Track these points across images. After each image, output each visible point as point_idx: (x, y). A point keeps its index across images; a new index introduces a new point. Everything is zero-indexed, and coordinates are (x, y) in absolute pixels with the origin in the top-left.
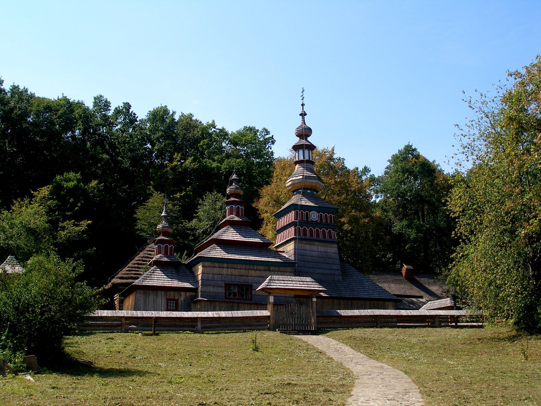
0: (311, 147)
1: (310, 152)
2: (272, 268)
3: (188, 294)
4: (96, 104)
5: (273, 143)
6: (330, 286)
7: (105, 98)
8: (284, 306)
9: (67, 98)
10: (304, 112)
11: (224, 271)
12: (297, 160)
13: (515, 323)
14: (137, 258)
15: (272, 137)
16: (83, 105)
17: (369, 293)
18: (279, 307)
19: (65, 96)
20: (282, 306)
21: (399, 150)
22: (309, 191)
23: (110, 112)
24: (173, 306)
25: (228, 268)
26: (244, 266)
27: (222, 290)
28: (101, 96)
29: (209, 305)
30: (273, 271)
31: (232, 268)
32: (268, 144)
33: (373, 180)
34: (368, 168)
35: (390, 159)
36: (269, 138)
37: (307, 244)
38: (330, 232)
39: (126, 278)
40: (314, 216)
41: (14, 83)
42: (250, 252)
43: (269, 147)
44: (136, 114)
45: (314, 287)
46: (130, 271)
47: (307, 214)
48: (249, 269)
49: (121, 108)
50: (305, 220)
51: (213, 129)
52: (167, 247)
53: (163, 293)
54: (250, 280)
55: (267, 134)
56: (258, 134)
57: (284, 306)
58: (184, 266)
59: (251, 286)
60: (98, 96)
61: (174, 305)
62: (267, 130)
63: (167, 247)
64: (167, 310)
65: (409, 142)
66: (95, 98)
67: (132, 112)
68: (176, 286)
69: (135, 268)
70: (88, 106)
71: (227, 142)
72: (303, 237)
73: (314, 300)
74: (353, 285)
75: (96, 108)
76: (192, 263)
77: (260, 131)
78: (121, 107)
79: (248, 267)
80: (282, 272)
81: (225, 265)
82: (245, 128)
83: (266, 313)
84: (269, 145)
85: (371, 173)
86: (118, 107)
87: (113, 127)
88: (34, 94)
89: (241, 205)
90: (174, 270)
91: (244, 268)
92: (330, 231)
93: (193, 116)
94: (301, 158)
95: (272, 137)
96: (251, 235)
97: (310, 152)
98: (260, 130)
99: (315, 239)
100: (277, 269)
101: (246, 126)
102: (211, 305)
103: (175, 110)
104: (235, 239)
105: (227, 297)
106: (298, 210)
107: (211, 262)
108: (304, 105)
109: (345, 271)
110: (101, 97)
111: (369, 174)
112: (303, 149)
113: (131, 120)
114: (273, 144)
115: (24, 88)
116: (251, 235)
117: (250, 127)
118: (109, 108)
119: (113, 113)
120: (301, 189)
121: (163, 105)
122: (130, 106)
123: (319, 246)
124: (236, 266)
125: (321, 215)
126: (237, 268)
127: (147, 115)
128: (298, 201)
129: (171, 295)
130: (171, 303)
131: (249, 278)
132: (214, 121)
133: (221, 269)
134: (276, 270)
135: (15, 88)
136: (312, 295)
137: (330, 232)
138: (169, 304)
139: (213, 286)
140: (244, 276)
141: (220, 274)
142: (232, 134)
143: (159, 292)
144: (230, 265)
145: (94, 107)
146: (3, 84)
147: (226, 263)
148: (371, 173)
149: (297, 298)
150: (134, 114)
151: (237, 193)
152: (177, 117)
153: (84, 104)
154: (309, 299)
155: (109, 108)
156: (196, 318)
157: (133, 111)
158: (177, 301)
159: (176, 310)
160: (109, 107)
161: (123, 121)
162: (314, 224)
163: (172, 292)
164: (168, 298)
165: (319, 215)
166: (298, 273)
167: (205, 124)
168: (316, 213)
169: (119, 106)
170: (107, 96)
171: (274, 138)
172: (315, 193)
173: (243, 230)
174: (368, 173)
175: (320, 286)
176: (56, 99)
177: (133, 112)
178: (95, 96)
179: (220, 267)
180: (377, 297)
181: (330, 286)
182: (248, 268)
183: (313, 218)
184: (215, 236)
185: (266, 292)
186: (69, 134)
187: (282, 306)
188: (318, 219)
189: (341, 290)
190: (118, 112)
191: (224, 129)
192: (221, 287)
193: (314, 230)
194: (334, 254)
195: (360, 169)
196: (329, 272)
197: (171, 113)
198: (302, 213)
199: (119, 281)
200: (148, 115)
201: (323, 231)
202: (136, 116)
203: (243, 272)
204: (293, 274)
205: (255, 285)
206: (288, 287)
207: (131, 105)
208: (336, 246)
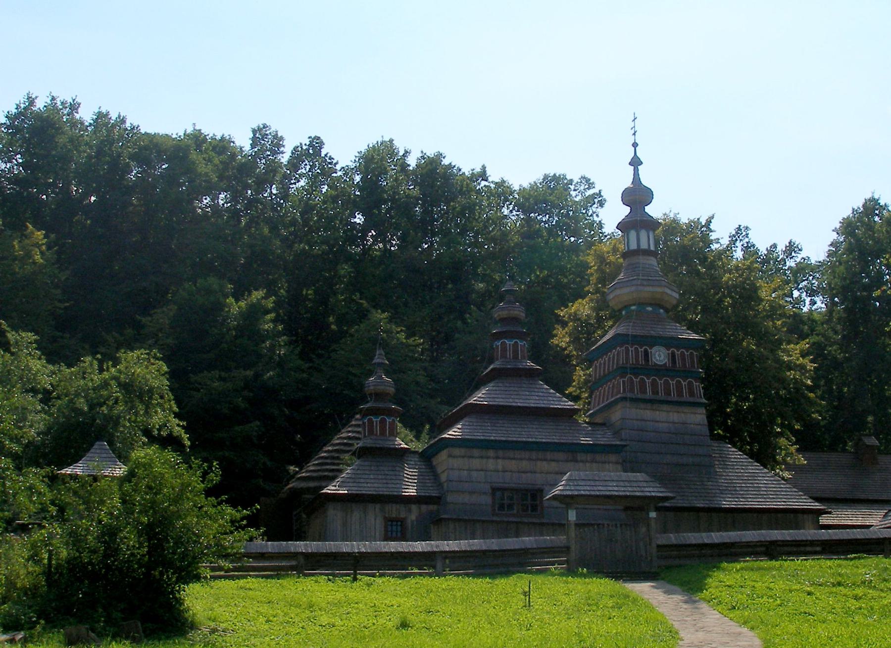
2: (580, 456)
3: (424, 508)
4: (255, 142)
5: (601, 204)
6: (693, 487)
9: (202, 132)
11: (491, 464)
15: (599, 194)
16: (232, 144)
19: (197, 128)
21: (853, 209)
22: (650, 309)
23: (283, 157)
25: (497, 458)
26: (527, 454)
27: (487, 500)
28: (265, 126)
30: (582, 461)
31: (504, 458)
32: (591, 206)
33: (804, 269)
34: (797, 243)
35: (838, 227)
36: (593, 196)
37: (647, 409)
38: (690, 383)
41: (100, 108)
43: (594, 213)
44: (333, 159)
48: (538, 459)
49: (304, 147)
51: (483, 183)
53: (378, 506)
54: (539, 480)
55: (589, 188)
56: (572, 187)
58: (417, 456)
60: (259, 127)
61: (399, 528)
62: (590, 180)
64: (387, 538)
65: (873, 193)
66: (254, 132)
67: (326, 155)
70: (242, 146)
71: (511, 207)
72: (639, 396)
73: (653, 515)
75: (256, 150)
77: (575, 182)
78: (305, 145)
79: (534, 455)
80: (599, 462)
81: (491, 453)
82: (546, 177)
84: (594, 210)
85: (803, 254)
86: (299, 145)
87: (292, 184)
88: (138, 126)
93: (444, 158)
94: (633, 246)
95: (599, 194)
96: (541, 394)
98: (576, 179)
99: (662, 399)
100: (589, 457)
101: (547, 173)
103: (408, 148)
105: (497, 511)
106: (628, 344)
107: (467, 447)
109: (721, 457)
110: (264, 127)
111: (798, 255)
113: (325, 167)
114: (602, 207)
115: (119, 116)
116: (541, 394)
117: (555, 175)
118: (282, 149)
119: (291, 156)
121: (387, 139)
122: (321, 144)
123: (670, 411)
124: (511, 454)
125: (673, 355)
126: (514, 459)
127: (355, 160)
128: (628, 327)
130: (392, 525)
131: (538, 475)
132: (484, 167)
133: (485, 460)
134: (589, 459)
135: (101, 117)
137: (690, 383)
139: (469, 492)
140: (527, 472)
141: (482, 470)
142: (520, 189)
143: (370, 506)
144: (500, 453)
145: (253, 146)
146: (79, 110)
147: (493, 449)
148: (803, 254)
149: (629, 512)
150: (329, 159)
152: (412, 162)
153: (233, 142)
154: (643, 512)
155: (282, 149)
157: (327, 153)
159: (403, 538)
160: (280, 148)
161: (309, 171)
162: (660, 371)
164: (387, 516)
165: (669, 354)
167: (467, 174)
168: (663, 349)
169: (301, 144)
170: (276, 126)
171: (602, 194)
173: (524, 385)
174: (798, 253)
175: (662, 490)
176: (181, 134)
177: (328, 155)
178: (255, 126)
179: (482, 457)
180: (782, 507)
181: (693, 487)
182: (534, 457)
183: (658, 358)
185: (561, 502)
186: (207, 200)
188: (666, 360)
189: (713, 495)
190: (298, 156)
191: (503, 181)
192: (485, 493)
193: (659, 382)
194: (699, 427)
195: (781, 247)
196: (691, 460)
197: (401, 153)
199: (448, 436)
200: (357, 160)
202: (334, 161)
203: (525, 465)
204: (619, 467)
205: (547, 488)
207: (324, 142)
208: (703, 410)
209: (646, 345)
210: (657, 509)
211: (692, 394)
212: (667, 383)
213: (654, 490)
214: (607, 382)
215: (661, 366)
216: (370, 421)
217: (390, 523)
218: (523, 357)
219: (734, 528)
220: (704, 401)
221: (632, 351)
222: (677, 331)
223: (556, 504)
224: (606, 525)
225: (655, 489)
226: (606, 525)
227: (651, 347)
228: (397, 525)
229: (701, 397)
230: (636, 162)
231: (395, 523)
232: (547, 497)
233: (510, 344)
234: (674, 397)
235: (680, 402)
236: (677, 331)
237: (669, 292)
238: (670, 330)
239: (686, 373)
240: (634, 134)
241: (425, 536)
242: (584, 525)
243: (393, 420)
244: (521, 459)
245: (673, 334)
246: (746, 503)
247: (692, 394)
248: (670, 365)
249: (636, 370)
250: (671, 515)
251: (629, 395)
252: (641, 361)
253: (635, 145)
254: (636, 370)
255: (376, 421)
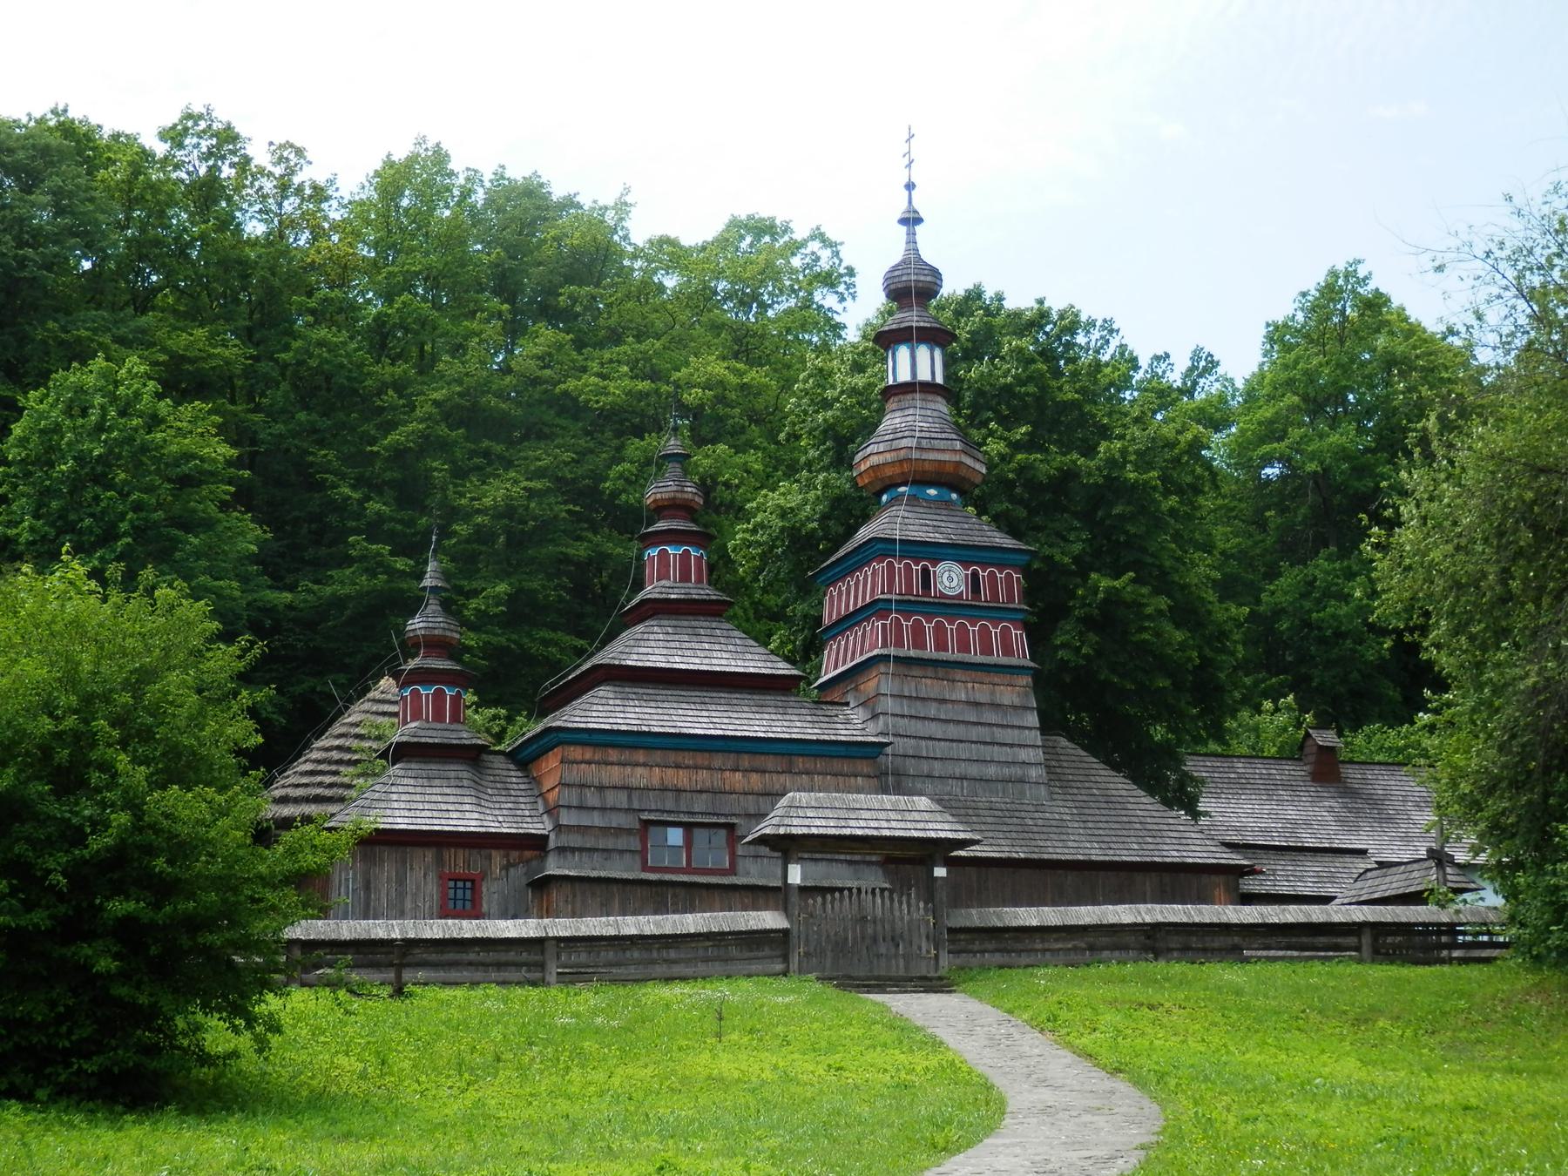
8: (846, 892)
10: (916, 212)
12: (891, 382)
13: (267, 847)
14: (337, 729)
17: (1145, 847)
18: (829, 897)
20: (837, 895)
22: (932, 492)
24: (464, 900)
38: (1005, 631)
39: (297, 801)
40: (950, 579)
46: (312, 773)
47: (925, 571)
53: (430, 855)
57: (846, 892)
61: (468, 893)
64: (444, 915)
68: (472, 829)
69: (330, 762)
74: (1090, 818)
76: (526, 753)
90: (465, 774)
102: (574, 896)
106: (894, 556)
125: (975, 575)
129: (458, 861)
130: (456, 888)
137: (1005, 631)
162: (950, 607)
163: (460, 852)
165: (967, 575)
183: (947, 584)
185: (773, 849)
187: (837, 895)
188: (963, 588)
201: (984, 629)
210: (951, 863)
211: (1008, 651)
212: (962, 630)
213: (943, 828)
216: (415, 693)
217: (451, 884)
219: (660, 909)
224: (855, 891)
225: (947, 826)
226: (855, 891)
227: (935, 562)
228: (464, 888)
229: (1025, 657)
230: (911, 220)
231: (460, 884)
233: (675, 555)
235: (989, 665)
237: (968, 461)
239: (996, 613)
240: (909, 166)
242: (367, 905)
243: (459, 693)
244: (696, 767)
248: (967, 596)
249: (907, 607)
250: (972, 871)
251: (892, 651)
252: (917, 587)
253: (910, 186)
254: (907, 607)
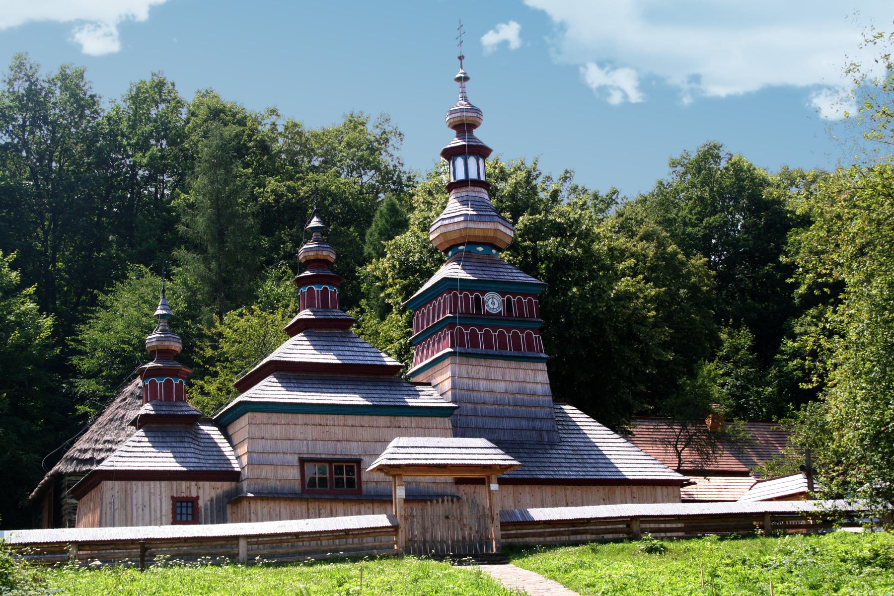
0: (482, 152)
1: (481, 161)
7: (188, 94)
22: (480, 249)
27: (294, 474)
29: (623, 492)
38: (529, 336)
40: (493, 303)
42: (353, 387)
45: (427, 459)
47: (477, 298)
50: (473, 314)
52: (168, 384)
54: (353, 450)
59: (358, 462)
63: (168, 384)
64: (175, 522)
72: (470, 350)
76: (225, 419)
83: (380, 520)
89: (331, 284)
91: (341, 423)
92: (529, 335)
94: (461, 176)
97: (481, 161)
99: (496, 353)
104: (369, 363)
105: (306, 488)
108: (463, 57)
112: (464, 156)
120: (463, 244)
125: (509, 300)
130: (181, 507)
136: (488, 477)
137: (529, 336)
138: (178, 510)
151: (322, 258)
156: (236, 538)
158: (194, 501)
165: (503, 301)
166: (460, 431)
172: (494, 251)
175: (506, 457)
183: (491, 306)
184: (273, 357)
185: (387, 474)
188: (501, 308)
193: (521, 335)
198: (466, 296)
205: (366, 459)
206: (435, 462)
208: (543, 366)
209: (509, 294)
210: (501, 482)
211: (530, 348)
213: (496, 457)
214: (437, 332)
215: (495, 315)
218: (334, 307)
220: (544, 355)
221: (461, 297)
222: (512, 274)
223: (381, 476)
229: (541, 351)
232: (371, 468)
233: (318, 291)
234: (510, 351)
236: (512, 274)
238: (505, 274)
241: (221, 519)
245: (508, 277)
246: (597, 473)
247: (530, 348)
252: (472, 309)
255: (161, 384)
